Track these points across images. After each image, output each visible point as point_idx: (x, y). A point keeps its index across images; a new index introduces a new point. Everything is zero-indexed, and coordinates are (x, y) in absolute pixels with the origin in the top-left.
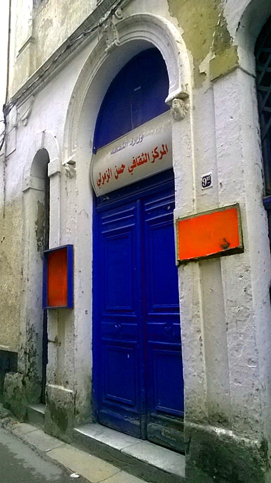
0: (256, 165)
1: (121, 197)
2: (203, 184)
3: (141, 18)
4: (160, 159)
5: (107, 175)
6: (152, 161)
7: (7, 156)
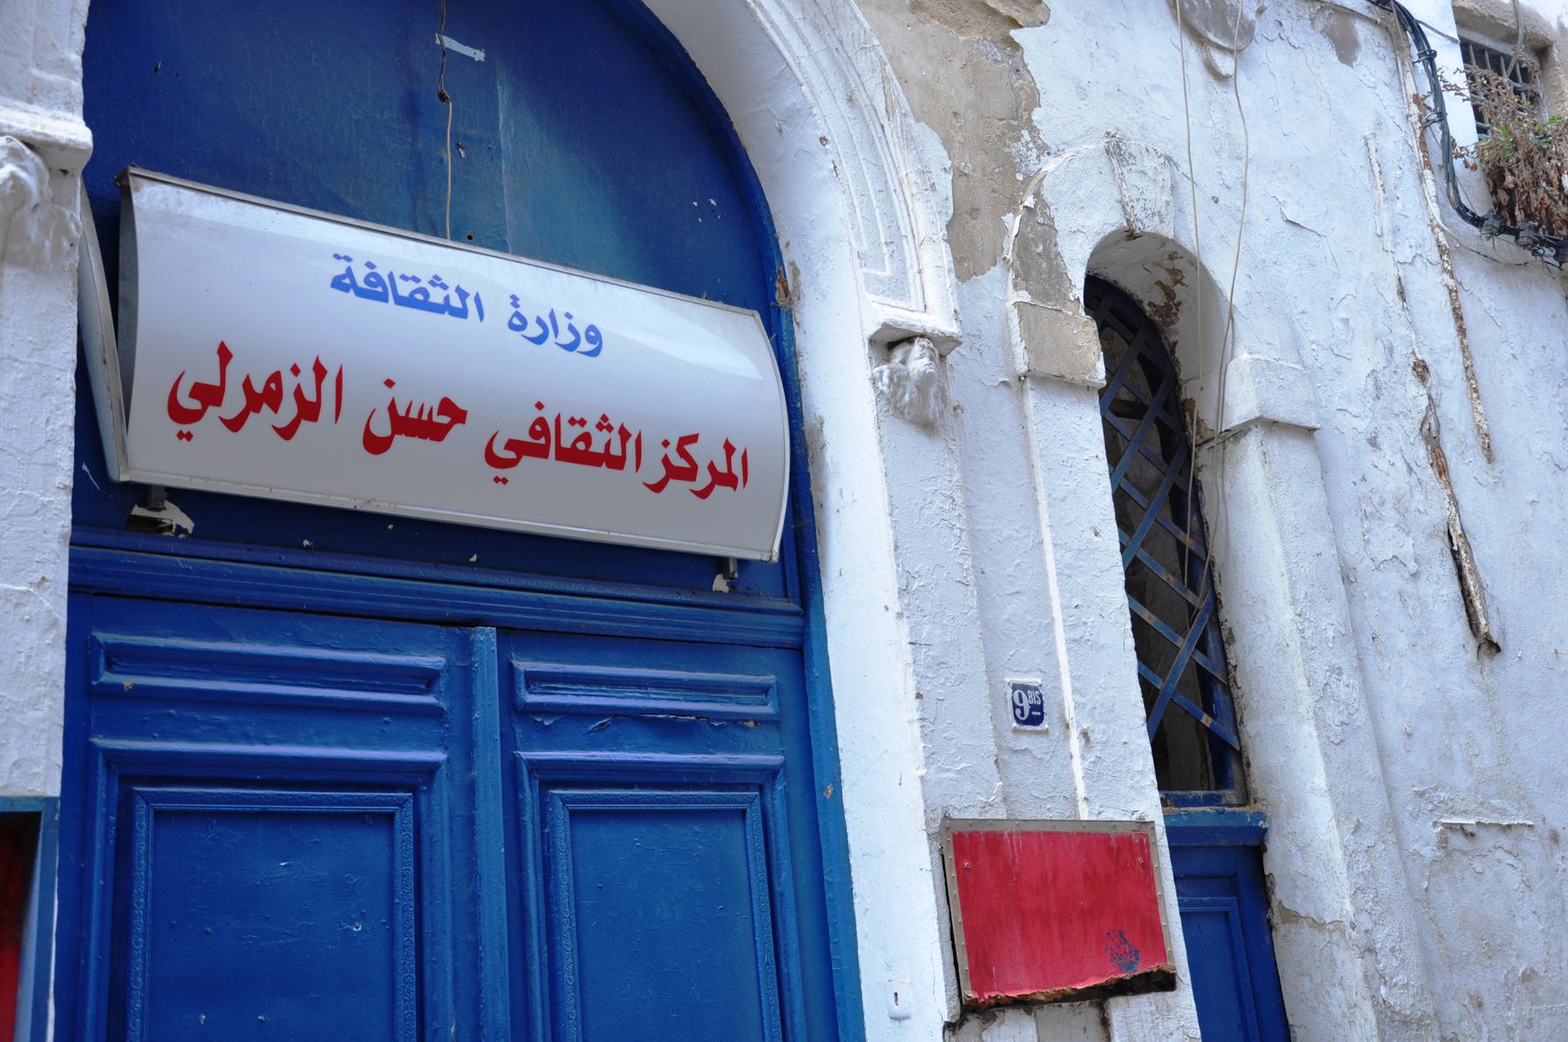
1: (312, 560)
2: (1018, 712)
4: (698, 493)
5: (298, 393)
6: (653, 481)
7: (75, 14)
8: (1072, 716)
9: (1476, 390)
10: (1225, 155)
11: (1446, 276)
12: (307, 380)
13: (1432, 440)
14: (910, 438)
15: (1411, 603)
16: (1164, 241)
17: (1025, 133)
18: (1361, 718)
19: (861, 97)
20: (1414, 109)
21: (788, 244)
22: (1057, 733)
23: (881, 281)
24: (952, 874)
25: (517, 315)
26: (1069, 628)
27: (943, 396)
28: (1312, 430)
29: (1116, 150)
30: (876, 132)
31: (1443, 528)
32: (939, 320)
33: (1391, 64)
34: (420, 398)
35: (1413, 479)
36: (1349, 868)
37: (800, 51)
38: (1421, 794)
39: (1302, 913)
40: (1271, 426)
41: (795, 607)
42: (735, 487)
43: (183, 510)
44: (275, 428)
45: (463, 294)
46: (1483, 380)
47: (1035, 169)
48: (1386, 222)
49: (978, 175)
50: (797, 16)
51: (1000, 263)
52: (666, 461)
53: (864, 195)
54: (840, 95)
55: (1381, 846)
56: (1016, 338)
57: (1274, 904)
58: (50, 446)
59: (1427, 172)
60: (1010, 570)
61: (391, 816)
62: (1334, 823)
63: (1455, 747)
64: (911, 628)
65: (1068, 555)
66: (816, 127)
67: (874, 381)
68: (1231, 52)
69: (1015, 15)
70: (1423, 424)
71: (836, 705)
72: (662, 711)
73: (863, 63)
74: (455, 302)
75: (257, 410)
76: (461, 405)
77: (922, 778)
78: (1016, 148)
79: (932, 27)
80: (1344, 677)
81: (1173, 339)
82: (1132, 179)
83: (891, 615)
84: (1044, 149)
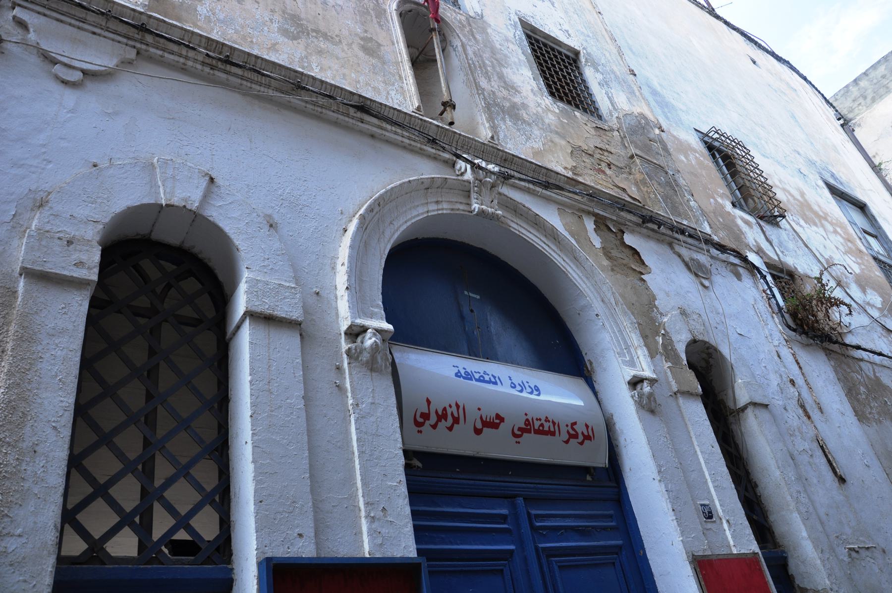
0: (204, 182)
3: (527, 213)
4: (579, 443)
5: (452, 414)
6: (565, 440)
8: (722, 514)
9: (811, 388)
10: (714, 313)
11: (790, 350)
12: (454, 408)
13: (803, 407)
14: (648, 416)
15: (813, 466)
16: (705, 342)
17: (654, 309)
18: (811, 509)
19: (606, 300)
20: (764, 294)
21: (586, 354)
22: (718, 522)
23: (626, 362)
24: (700, 576)
25: (512, 383)
26: (713, 482)
27: (655, 401)
28: (767, 405)
29: (683, 313)
30: (613, 311)
31: (815, 438)
32: (648, 373)
33: (753, 280)
34: (489, 413)
35: (801, 421)
36: (824, 566)
37: (584, 286)
38: (837, 537)
39: (809, 588)
40: (755, 404)
41: (615, 485)
42: (591, 440)
43: (418, 460)
44: (447, 427)
45: (495, 377)
46: (812, 386)
47: (661, 321)
48: (767, 332)
49: (644, 324)
50: (581, 275)
51: (659, 354)
52: (568, 432)
53: (614, 333)
54: (599, 299)
55: (831, 558)
56: (671, 379)
57: (796, 586)
58: (394, 433)
59: (774, 315)
60: (689, 462)
61: (502, 570)
62: (814, 550)
63: (842, 518)
64: (665, 485)
65: (706, 455)
66: (594, 311)
67: (632, 397)
68: (707, 279)
69: (641, 271)
70: (798, 401)
71: (637, 520)
72: (581, 526)
73: (605, 289)
74: (493, 380)
75: (441, 421)
76: (502, 415)
77: (682, 540)
78: (653, 314)
79: (619, 276)
80: (802, 494)
81: (710, 378)
82: (691, 322)
83: (657, 481)
84: (661, 314)
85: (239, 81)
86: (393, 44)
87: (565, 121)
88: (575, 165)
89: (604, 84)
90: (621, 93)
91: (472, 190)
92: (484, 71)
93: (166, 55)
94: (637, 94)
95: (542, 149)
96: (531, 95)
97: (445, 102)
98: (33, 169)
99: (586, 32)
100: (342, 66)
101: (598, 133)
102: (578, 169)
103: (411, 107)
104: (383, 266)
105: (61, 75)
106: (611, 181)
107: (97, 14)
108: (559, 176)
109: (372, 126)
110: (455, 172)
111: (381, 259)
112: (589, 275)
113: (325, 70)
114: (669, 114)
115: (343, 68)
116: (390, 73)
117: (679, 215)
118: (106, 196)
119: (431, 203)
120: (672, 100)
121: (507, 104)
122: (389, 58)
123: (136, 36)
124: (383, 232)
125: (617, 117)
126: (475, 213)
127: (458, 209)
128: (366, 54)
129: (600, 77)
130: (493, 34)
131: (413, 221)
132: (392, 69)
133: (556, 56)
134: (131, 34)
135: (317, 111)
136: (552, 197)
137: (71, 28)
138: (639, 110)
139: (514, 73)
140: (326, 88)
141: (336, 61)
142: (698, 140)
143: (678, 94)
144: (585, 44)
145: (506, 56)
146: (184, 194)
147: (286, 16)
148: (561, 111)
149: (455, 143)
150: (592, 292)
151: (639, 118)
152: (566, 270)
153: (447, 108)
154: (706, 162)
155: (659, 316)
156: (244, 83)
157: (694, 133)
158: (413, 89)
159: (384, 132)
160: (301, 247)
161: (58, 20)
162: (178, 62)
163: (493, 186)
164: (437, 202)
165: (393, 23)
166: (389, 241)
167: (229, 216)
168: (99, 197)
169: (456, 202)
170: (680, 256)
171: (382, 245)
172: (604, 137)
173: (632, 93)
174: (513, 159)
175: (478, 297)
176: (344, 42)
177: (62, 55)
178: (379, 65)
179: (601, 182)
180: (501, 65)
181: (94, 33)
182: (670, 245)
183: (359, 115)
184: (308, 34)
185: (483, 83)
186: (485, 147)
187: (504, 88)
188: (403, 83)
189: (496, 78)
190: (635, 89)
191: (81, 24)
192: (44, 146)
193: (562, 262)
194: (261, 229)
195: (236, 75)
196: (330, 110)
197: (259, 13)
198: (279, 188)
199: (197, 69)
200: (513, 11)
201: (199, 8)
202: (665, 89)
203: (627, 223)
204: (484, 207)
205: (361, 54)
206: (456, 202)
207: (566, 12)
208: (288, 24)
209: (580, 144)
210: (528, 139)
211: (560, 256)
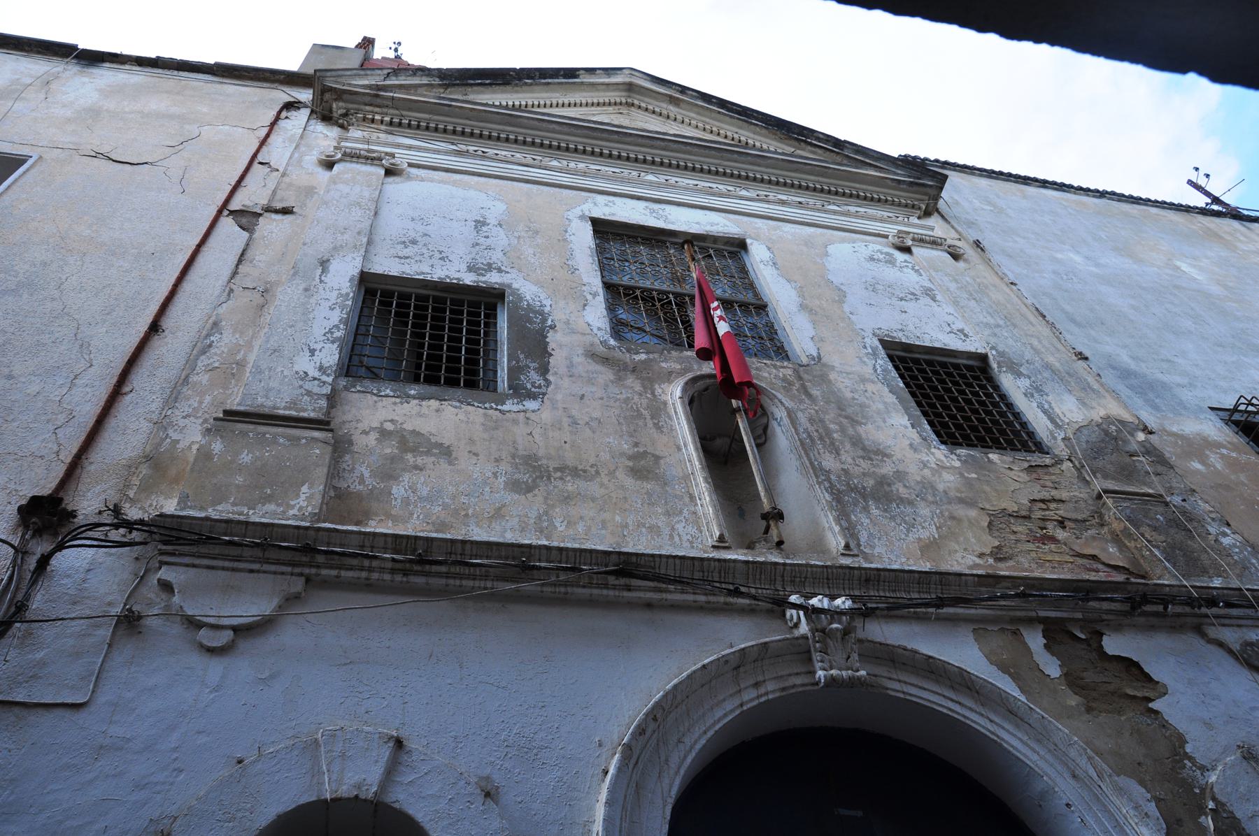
0: (386, 751)
17: (1186, 762)
37: (1035, 757)
69: (1147, 695)
73: (1073, 753)
78: (1185, 773)
79: (1103, 718)
84: (1203, 769)
85: (443, 581)
86: (679, 449)
87: (974, 476)
88: (997, 543)
89: (1036, 390)
90: (1066, 397)
91: (812, 649)
92: (828, 443)
93: (343, 573)
94: (1096, 386)
95: (936, 536)
96: (910, 454)
97: (765, 514)
98: (158, 788)
99: (992, 321)
100: (601, 510)
101: (1035, 475)
102: (1005, 550)
103: (709, 540)
104: (669, 818)
105: (205, 642)
106: (1067, 551)
107: (252, 547)
108: (963, 578)
109: (645, 591)
110: (786, 623)
111: (664, 806)
112: (1041, 736)
113: (575, 524)
114: (1157, 401)
115: (601, 513)
116: (676, 496)
117: (1204, 571)
118: (249, 805)
119: (746, 688)
120: (1160, 376)
121: (870, 483)
122: (674, 473)
123: (304, 559)
124: (667, 760)
125: (1063, 439)
126: (822, 684)
127: (794, 686)
128: (636, 480)
129: (1024, 383)
130: (840, 379)
131: (717, 727)
132: (679, 489)
133: (950, 375)
134: (297, 559)
135: (560, 593)
136: (959, 614)
137: (224, 573)
138: (1102, 413)
139: (878, 428)
140: (567, 557)
141: (592, 504)
142: (1220, 424)
143: (1169, 361)
144: (993, 340)
145: (862, 406)
146: (357, 777)
147: (517, 461)
148: (964, 462)
149: (779, 578)
150: (1051, 765)
151: (1104, 426)
152: (998, 736)
153: (771, 522)
154: (1244, 458)
155: (1198, 772)
156: (451, 581)
157: (1212, 416)
158: (711, 511)
159: (664, 596)
160: (536, 817)
161: (208, 567)
162: (359, 578)
163: (846, 632)
164: (757, 685)
165: (678, 419)
166: (677, 773)
167: (423, 795)
168: (240, 810)
169: (790, 675)
170: (1221, 645)
171: (666, 781)
172: (1047, 477)
173: (1086, 388)
174: (879, 575)
175: (860, 814)
176: (604, 472)
177: (206, 616)
178: (658, 489)
179: (1049, 558)
180: (854, 422)
181: (252, 571)
182: (1199, 630)
183: (623, 581)
184: (549, 478)
185: (829, 462)
186: (830, 570)
187: (863, 458)
188: (696, 505)
189: (848, 446)
190: (1090, 379)
191: (236, 565)
192: (175, 749)
193: (989, 726)
194: (472, 804)
195: (439, 575)
196: (578, 586)
197: (478, 469)
198: (503, 730)
199: (385, 581)
200: (869, 333)
201: (394, 491)
202: (1144, 362)
203: (1105, 617)
204: (833, 672)
205: (629, 482)
206: (790, 675)
207: (956, 303)
208: (520, 473)
209: (1004, 505)
210: (911, 526)
211: (982, 715)
